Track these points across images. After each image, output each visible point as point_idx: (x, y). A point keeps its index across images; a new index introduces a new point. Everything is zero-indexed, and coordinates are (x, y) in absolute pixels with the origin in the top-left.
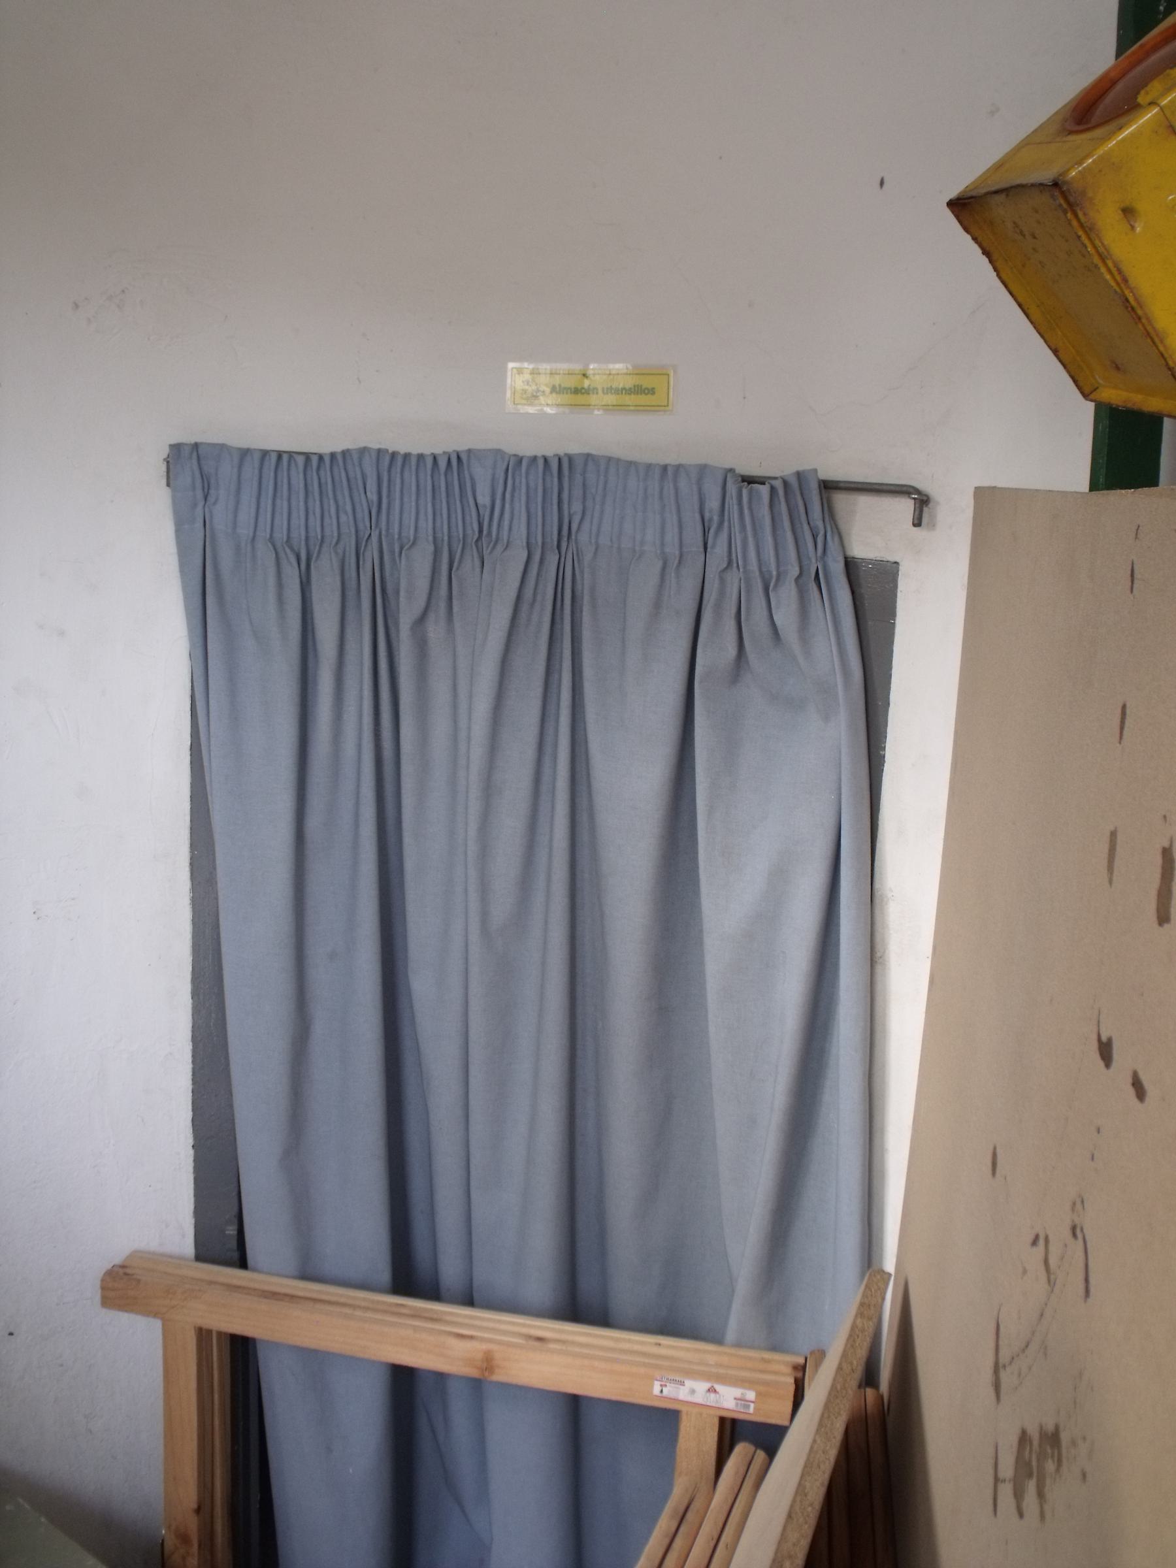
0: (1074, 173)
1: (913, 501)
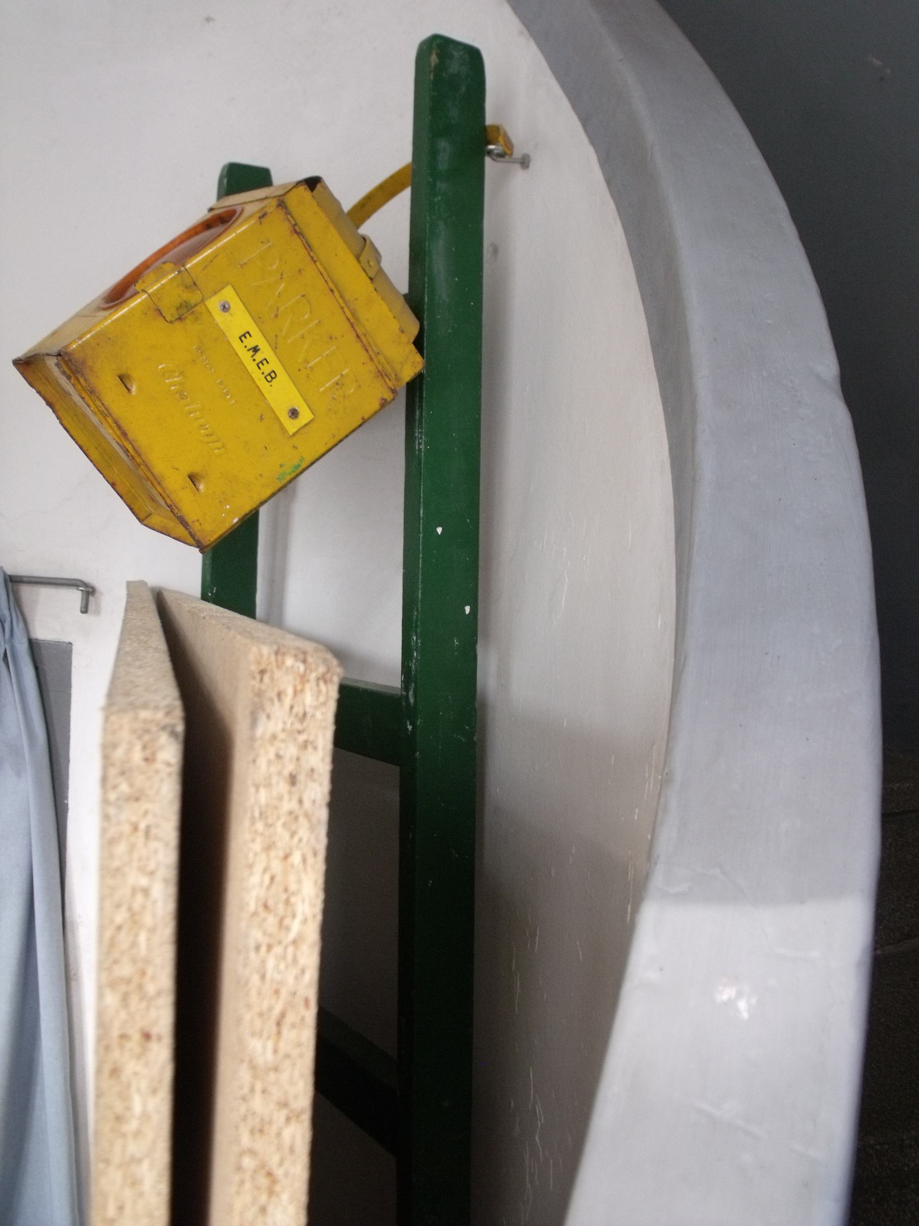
0: (75, 346)
1: (80, 592)
